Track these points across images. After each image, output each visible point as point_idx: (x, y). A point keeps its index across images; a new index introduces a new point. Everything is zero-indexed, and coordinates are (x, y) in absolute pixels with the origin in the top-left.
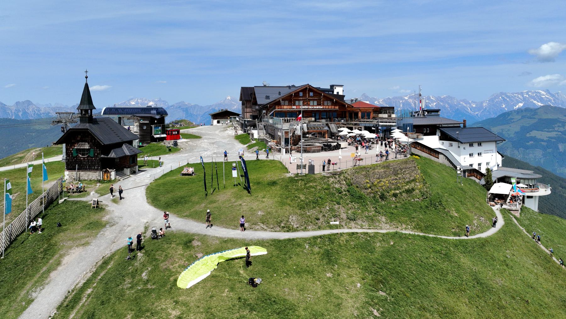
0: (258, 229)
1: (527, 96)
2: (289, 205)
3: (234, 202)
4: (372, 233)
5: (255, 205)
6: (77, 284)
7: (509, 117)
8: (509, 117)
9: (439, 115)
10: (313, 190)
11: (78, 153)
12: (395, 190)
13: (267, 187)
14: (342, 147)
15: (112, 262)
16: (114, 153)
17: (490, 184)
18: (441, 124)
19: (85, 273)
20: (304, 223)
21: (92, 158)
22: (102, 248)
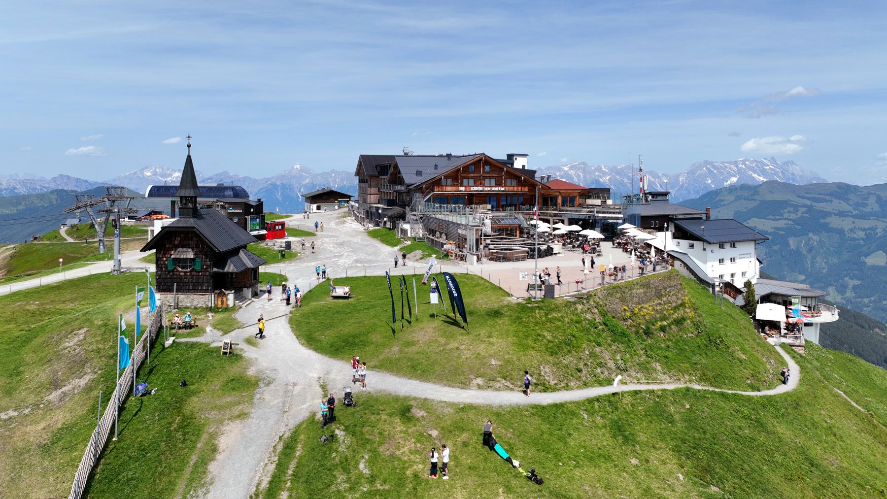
0: (500, 387)
1: (744, 167)
2: (533, 348)
3: (445, 345)
4: (658, 390)
5: (482, 349)
6: (259, 484)
7: (717, 199)
8: (717, 199)
9: (668, 200)
10: (559, 323)
11: (176, 265)
12: (661, 320)
13: (488, 320)
14: (554, 252)
15: (300, 446)
16: (232, 265)
17: (753, 305)
18: (676, 215)
19: (262, 464)
20: (562, 376)
21: (199, 272)
22: (271, 422)
